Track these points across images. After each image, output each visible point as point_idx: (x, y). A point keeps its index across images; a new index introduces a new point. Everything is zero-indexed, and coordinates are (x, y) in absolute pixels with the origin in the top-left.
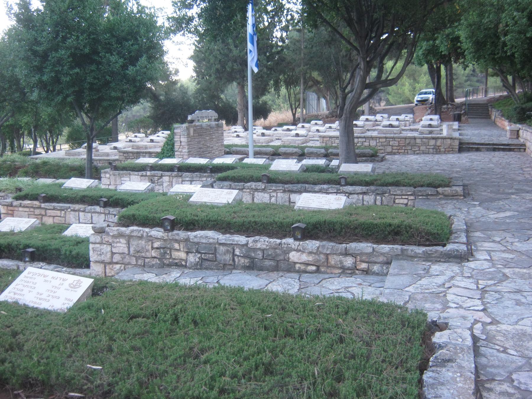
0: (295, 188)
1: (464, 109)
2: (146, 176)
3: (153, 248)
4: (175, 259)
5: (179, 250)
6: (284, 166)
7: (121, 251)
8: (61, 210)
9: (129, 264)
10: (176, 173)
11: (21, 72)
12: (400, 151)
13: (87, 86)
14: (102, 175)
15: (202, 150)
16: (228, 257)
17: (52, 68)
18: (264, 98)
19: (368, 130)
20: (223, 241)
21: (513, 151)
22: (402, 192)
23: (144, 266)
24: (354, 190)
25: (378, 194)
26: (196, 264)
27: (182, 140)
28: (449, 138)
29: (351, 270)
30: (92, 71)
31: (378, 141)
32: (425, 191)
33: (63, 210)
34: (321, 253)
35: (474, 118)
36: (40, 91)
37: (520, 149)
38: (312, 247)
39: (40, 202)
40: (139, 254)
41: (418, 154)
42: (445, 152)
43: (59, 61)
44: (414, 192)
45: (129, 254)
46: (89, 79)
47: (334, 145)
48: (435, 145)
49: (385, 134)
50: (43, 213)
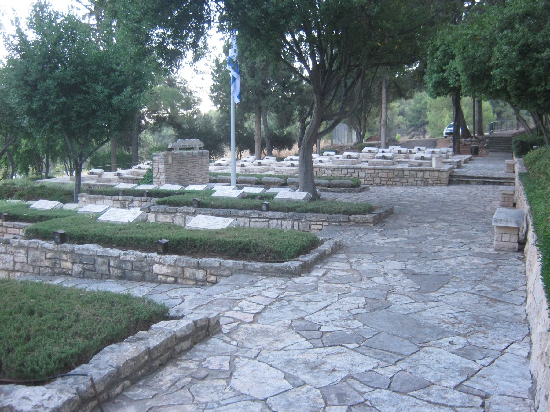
0: (222, 212)
1: (487, 143)
2: (118, 200)
3: (46, 258)
4: (63, 268)
5: (66, 261)
6: (227, 193)
7: (21, 261)
8: (20, 228)
9: (27, 272)
10: (145, 198)
11: (12, 100)
12: (388, 183)
13: (74, 114)
14: (79, 199)
15: (182, 177)
16: (104, 268)
17: (41, 97)
18: (289, 129)
19: (399, 162)
20: (100, 254)
21: (504, 185)
22: (317, 218)
23: (39, 274)
24: (274, 216)
25: (295, 220)
26: (80, 273)
27: (160, 167)
28: (437, 171)
29: (202, 282)
30: (80, 100)
31: (367, 172)
32: (337, 218)
33: (22, 228)
34: (178, 266)
35: (496, 152)
36: (31, 118)
37: (510, 182)
38: (170, 260)
39: (3, 221)
40: (35, 263)
41: (406, 186)
42: (433, 185)
43: (47, 91)
44: (328, 218)
45: (27, 263)
46: (76, 108)
47: (324, 175)
48: (423, 178)
49: (375, 165)
50: (5, 231)
